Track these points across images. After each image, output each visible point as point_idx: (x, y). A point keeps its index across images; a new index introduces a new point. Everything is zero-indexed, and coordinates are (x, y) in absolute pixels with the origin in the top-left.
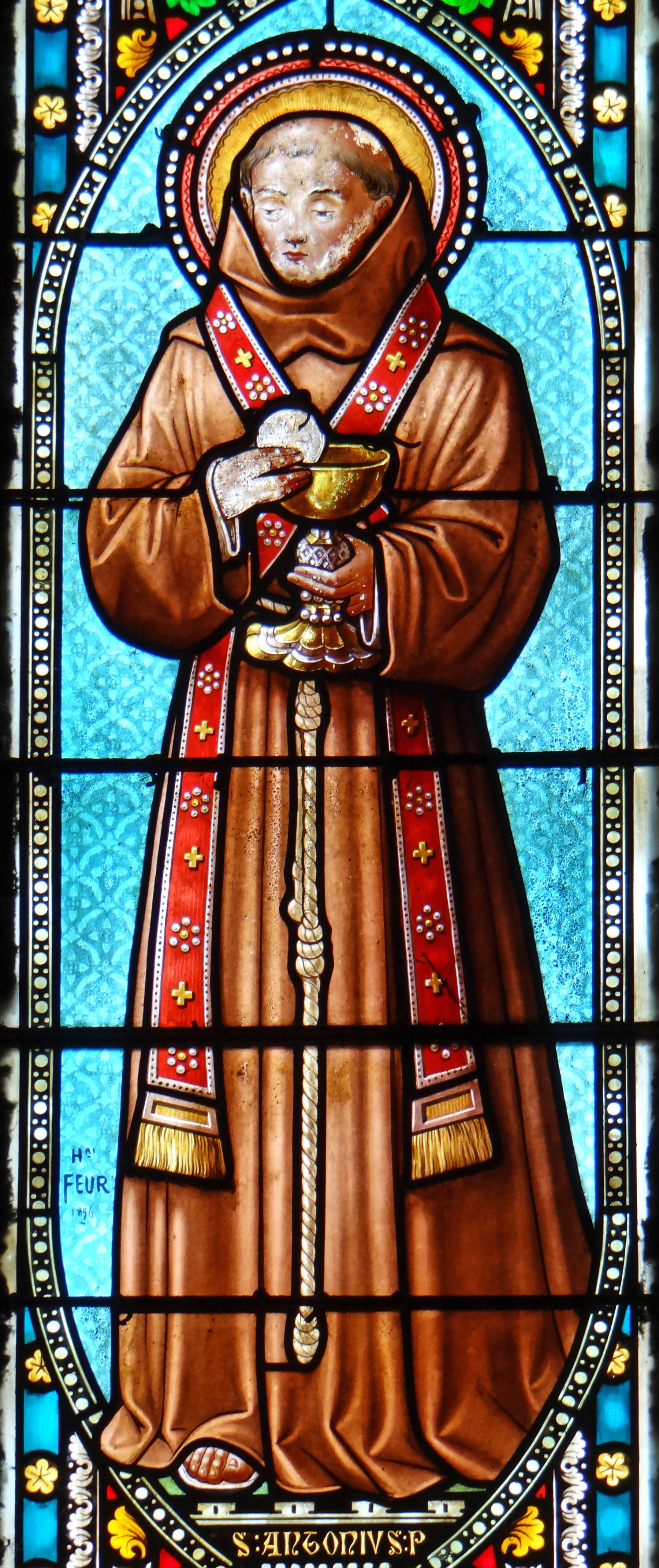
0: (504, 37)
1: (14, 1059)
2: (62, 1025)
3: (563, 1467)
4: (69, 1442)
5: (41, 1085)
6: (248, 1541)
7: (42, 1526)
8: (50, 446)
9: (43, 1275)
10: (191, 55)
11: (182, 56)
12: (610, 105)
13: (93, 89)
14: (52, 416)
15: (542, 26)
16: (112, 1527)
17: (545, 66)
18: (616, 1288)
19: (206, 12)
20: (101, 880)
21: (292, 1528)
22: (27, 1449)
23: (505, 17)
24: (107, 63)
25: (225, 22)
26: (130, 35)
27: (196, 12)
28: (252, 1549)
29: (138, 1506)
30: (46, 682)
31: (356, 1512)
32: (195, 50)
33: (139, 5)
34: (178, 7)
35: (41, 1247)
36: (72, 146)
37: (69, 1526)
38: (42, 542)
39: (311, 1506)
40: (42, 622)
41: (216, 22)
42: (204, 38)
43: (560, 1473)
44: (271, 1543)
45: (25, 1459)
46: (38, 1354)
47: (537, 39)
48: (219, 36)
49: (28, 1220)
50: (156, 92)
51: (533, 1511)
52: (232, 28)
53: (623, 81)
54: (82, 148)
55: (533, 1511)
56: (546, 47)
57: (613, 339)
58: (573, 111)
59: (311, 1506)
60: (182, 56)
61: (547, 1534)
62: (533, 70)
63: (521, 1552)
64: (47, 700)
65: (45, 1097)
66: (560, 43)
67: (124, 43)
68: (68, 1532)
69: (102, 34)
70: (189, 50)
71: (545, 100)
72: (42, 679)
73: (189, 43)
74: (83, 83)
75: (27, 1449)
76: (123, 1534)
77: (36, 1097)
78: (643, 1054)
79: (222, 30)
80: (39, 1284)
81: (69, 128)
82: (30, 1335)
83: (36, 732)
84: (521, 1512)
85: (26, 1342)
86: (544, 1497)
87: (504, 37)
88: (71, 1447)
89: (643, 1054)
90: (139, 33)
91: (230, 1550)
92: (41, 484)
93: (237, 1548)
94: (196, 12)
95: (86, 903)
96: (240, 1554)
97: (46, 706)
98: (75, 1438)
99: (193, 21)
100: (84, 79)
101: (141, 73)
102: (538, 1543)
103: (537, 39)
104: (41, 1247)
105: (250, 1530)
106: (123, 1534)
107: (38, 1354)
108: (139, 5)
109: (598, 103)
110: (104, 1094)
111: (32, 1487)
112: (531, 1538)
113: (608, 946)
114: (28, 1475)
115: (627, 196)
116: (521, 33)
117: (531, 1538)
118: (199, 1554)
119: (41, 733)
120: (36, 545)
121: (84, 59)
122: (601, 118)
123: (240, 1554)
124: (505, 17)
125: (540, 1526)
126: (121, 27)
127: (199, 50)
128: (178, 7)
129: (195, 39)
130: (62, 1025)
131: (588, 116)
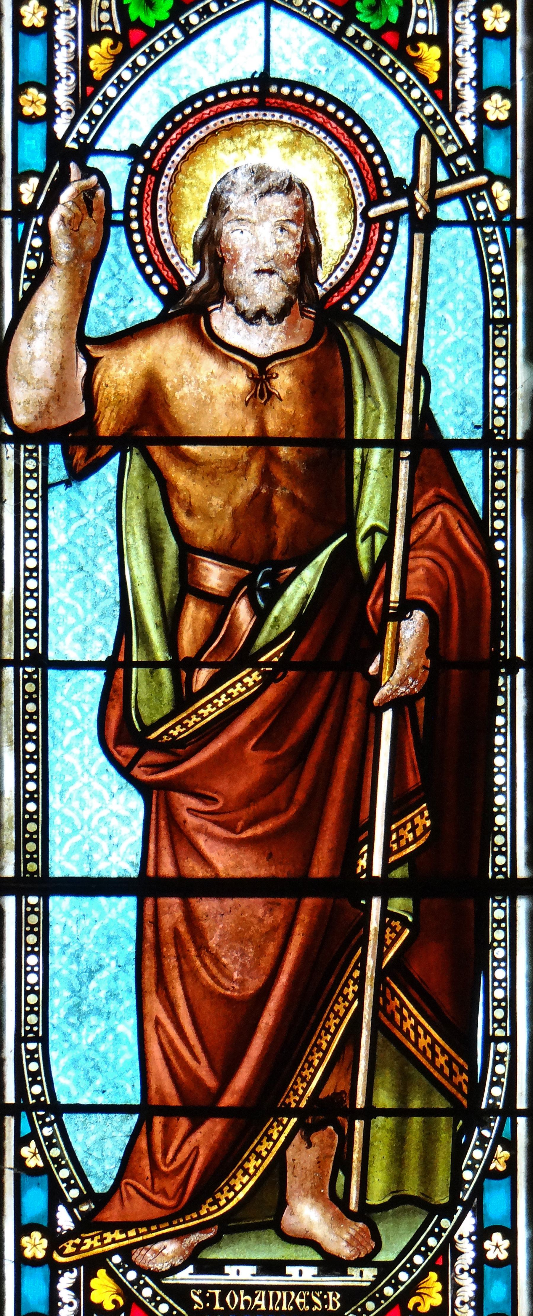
0: (409, 50)
1: (9, 903)
2: (51, 875)
3: (456, 1237)
4: (57, 1211)
5: (32, 979)
6: (202, 1297)
7: (36, 1287)
8: (37, 558)
9: (37, 1090)
10: (149, 60)
11: (142, 61)
12: (496, 108)
13: (68, 86)
14: (39, 946)
15: (439, 40)
16: (94, 1283)
17: (443, 73)
18: (495, 453)
19: (160, 25)
20: (81, 757)
21: (237, 1288)
22: (20, 170)
23: (409, 33)
24: (80, 63)
25: (177, 33)
26: (99, 43)
27: (152, 24)
28: (205, 1305)
29: (114, 1268)
30: (35, 595)
31: (290, 1275)
32: (152, 57)
33: (105, 4)
34: (138, 20)
35: (33, 1067)
36: (51, 134)
37: (59, 1287)
38: (31, 477)
39: (253, 1269)
40: (32, 979)
41: (170, 33)
42: (160, 46)
43: (454, 1243)
44: (260, 1299)
45: (19, 178)
46: (33, 1144)
47: (436, 52)
48: (172, 45)
49: (23, 1045)
50: (119, 91)
51: (433, 1276)
52: (183, 38)
53: (508, 175)
54: (60, 136)
55: (433, 1276)
56: (443, 59)
57: (499, 307)
58: (467, 115)
59: (253, 1269)
60: (142, 61)
61: (444, 1293)
62: (433, 78)
63: (424, 1308)
64: (36, 609)
65: (35, 554)
66: (455, 57)
67: (93, 50)
68: (58, 1291)
69: (76, 41)
70: (147, 55)
71: (443, 104)
72: (32, 932)
73: (147, 51)
74: (60, 80)
75: (20, 170)
76: (103, 1291)
77: (28, 554)
78: (520, 453)
79: (174, 40)
80: (34, 1096)
81: (50, 117)
82: (25, 1130)
83: (27, 636)
84: (424, 1275)
85: (22, 1135)
86: (442, 1262)
87: (409, 50)
88: (58, 1215)
89: (520, 453)
90: (107, 42)
91: (187, 1303)
92: (29, 873)
93: (194, 1302)
94: (152, 24)
95: (69, 723)
96: (196, 1307)
97: (35, 717)
98: (61, 1208)
99: (151, 32)
100: (61, 78)
101: (107, 77)
102: (437, 1300)
103: (436, 52)
104: (33, 1067)
105: (205, 1287)
106: (103, 1291)
107: (33, 1144)
108: (105, 4)
109: (487, 105)
110: (84, 988)
111: (28, 1254)
112: (432, 1296)
113: (495, 964)
114: (21, 102)
115: (510, 183)
116: (423, 46)
117: (432, 1296)
118: (164, 1308)
119: (32, 637)
120: (26, 479)
121: (61, 60)
122: (491, 117)
123: (196, 1307)
124: (409, 33)
125: (439, 1286)
126: (91, 38)
127: (155, 57)
128: (138, 20)
129: (152, 47)
130: (51, 875)
131: (480, 115)
